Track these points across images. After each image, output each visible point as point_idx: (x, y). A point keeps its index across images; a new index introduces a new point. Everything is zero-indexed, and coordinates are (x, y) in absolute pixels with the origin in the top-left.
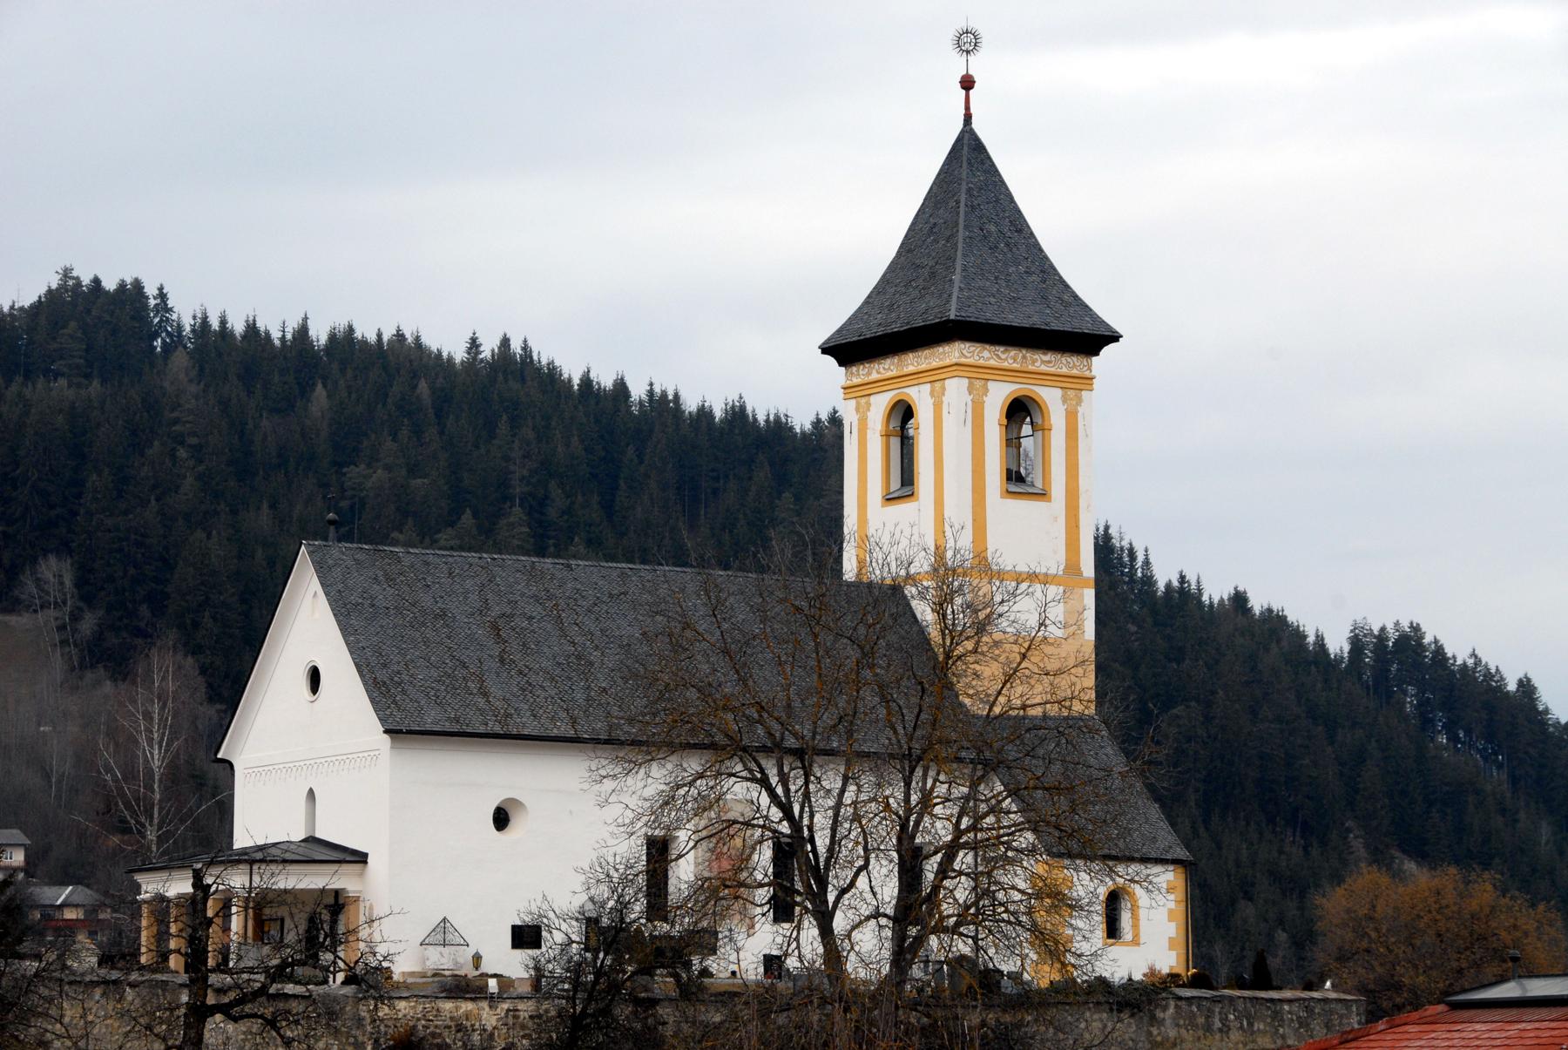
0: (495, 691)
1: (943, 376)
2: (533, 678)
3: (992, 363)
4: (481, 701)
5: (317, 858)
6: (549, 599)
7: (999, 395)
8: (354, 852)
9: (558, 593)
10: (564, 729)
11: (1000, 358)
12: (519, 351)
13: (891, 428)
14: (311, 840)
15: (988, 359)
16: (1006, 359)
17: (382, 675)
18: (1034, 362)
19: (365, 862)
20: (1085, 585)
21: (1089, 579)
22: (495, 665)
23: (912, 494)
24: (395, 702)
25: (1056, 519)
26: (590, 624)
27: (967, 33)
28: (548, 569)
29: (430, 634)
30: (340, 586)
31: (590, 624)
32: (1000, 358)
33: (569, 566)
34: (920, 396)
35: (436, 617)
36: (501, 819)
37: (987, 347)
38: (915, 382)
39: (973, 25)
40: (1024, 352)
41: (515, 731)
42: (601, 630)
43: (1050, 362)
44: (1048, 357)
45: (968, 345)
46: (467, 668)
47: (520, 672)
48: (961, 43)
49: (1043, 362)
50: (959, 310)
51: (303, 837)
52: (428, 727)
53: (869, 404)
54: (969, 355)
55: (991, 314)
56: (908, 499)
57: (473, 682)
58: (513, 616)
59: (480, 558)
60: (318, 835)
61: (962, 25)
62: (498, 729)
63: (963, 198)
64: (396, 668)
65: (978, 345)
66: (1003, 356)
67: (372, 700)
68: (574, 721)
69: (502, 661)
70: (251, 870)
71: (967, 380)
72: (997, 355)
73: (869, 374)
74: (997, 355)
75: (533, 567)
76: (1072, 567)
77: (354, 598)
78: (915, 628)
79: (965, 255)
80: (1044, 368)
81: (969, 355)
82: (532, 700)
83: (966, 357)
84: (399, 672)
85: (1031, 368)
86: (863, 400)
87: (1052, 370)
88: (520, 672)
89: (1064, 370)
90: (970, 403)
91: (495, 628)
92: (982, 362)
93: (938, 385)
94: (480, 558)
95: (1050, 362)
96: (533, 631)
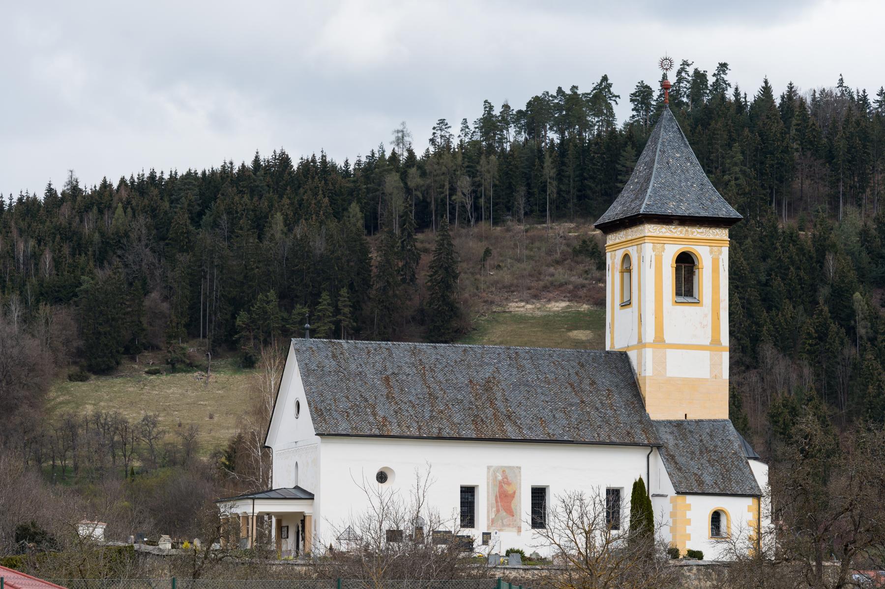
0: (381, 413)
1: (641, 242)
2: (403, 406)
3: (668, 235)
4: (371, 419)
5: (287, 497)
6: (421, 365)
7: (671, 252)
8: (310, 494)
9: (425, 361)
10: (414, 431)
11: (672, 232)
12: (733, 98)
13: (624, 268)
14: (297, 488)
15: (665, 232)
16: (676, 232)
17: (321, 406)
18: (692, 233)
19: (313, 499)
20: (723, 350)
21: (725, 347)
22: (383, 399)
23: (630, 303)
24: (325, 420)
25: (706, 316)
26: (440, 377)
27: (666, 59)
28: (423, 349)
29: (351, 384)
30: (307, 361)
31: (440, 377)
32: (672, 232)
33: (435, 347)
34: (633, 251)
35: (356, 375)
36: (382, 477)
37: (665, 226)
38: (631, 245)
39: (669, 56)
40: (687, 228)
41: (386, 433)
42: (446, 380)
43: (702, 233)
44: (702, 230)
45: (652, 226)
46: (367, 401)
47: (396, 403)
48: (663, 65)
49: (698, 233)
50: (645, 208)
51: (294, 486)
52: (339, 432)
53: (615, 255)
54: (653, 231)
55: (671, 208)
56: (628, 306)
57: (369, 409)
58: (398, 374)
59: (386, 344)
60: (299, 485)
61: (663, 56)
62: (377, 432)
63: (659, 146)
64: (329, 402)
65: (659, 226)
66: (674, 231)
67: (313, 419)
68: (420, 428)
69: (388, 398)
70: (254, 502)
71: (652, 244)
72: (671, 231)
73: (615, 239)
74: (671, 231)
75: (415, 348)
76: (716, 341)
77: (314, 367)
78: (629, 375)
79: (656, 178)
80: (699, 236)
81: (653, 231)
82: (399, 417)
83: (652, 232)
84: (330, 404)
85: (691, 236)
86: (613, 253)
87: (704, 237)
88: (396, 403)
89: (711, 237)
90: (653, 257)
91: (387, 379)
92: (661, 235)
93: (639, 246)
94: (386, 344)
95: (702, 233)
96: (408, 382)
